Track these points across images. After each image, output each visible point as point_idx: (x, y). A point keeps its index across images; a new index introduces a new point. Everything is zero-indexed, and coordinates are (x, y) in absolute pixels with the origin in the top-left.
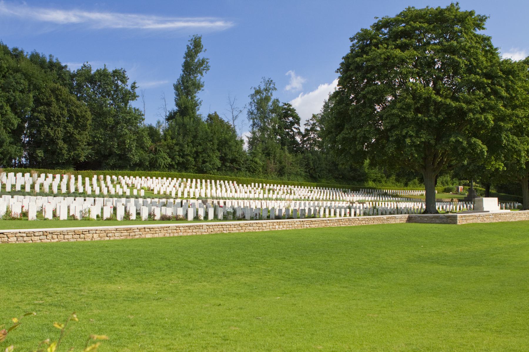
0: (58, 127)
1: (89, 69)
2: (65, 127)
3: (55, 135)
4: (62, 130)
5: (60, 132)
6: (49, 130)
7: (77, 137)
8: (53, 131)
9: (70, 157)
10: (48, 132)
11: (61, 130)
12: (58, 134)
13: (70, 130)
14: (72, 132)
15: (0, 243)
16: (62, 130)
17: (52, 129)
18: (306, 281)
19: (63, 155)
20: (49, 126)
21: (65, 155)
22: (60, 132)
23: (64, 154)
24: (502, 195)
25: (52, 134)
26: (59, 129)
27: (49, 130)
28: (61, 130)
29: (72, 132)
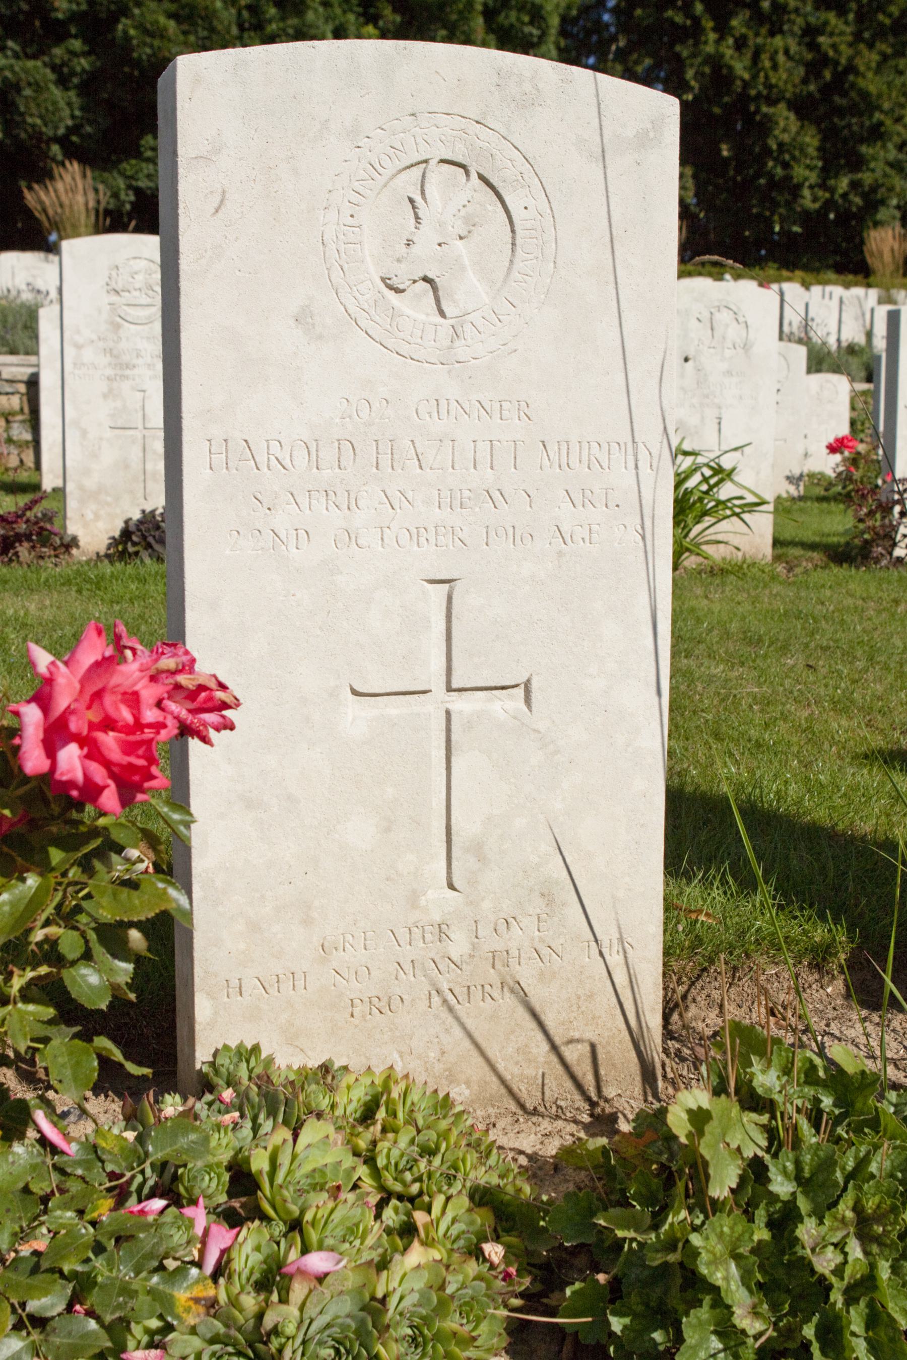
0: (772, 34)
1: (113, 538)
2: (810, 33)
3: (755, 77)
4: (794, 48)
5: (781, 58)
6: (728, 51)
7: (872, 84)
8: (747, 60)
9: (829, 204)
10: (716, 63)
11: (787, 52)
12: (775, 67)
13: (834, 46)
14: (843, 61)
15: (16, 1344)
16: (794, 48)
17: (740, 44)
18: (840, 1246)
19: (795, 190)
20: (722, 29)
21: (806, 192)
22: (781, 58)
23: (799, 186)
24: (895, 890)
25: (740, 68)
26: (778, 41)
27: (728, 51)
28: (787, 52)
29: (843, 61)
